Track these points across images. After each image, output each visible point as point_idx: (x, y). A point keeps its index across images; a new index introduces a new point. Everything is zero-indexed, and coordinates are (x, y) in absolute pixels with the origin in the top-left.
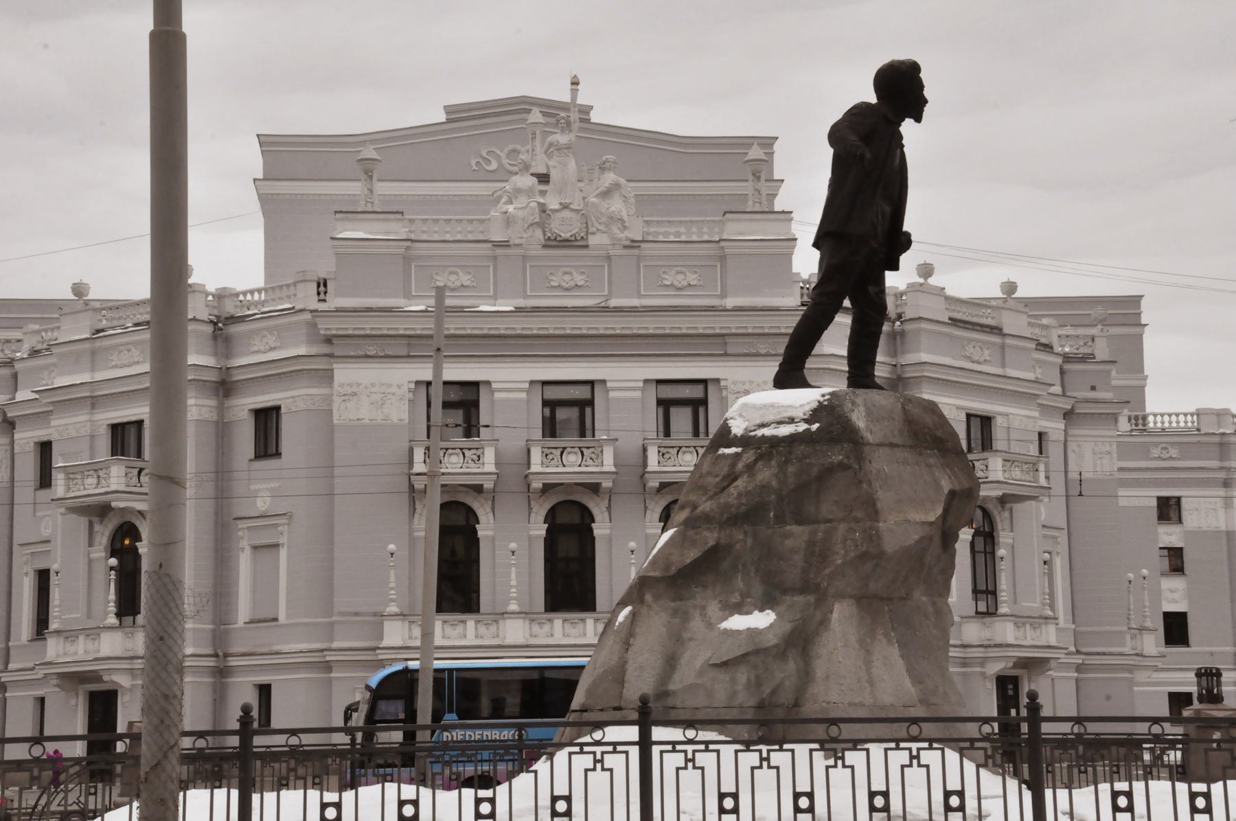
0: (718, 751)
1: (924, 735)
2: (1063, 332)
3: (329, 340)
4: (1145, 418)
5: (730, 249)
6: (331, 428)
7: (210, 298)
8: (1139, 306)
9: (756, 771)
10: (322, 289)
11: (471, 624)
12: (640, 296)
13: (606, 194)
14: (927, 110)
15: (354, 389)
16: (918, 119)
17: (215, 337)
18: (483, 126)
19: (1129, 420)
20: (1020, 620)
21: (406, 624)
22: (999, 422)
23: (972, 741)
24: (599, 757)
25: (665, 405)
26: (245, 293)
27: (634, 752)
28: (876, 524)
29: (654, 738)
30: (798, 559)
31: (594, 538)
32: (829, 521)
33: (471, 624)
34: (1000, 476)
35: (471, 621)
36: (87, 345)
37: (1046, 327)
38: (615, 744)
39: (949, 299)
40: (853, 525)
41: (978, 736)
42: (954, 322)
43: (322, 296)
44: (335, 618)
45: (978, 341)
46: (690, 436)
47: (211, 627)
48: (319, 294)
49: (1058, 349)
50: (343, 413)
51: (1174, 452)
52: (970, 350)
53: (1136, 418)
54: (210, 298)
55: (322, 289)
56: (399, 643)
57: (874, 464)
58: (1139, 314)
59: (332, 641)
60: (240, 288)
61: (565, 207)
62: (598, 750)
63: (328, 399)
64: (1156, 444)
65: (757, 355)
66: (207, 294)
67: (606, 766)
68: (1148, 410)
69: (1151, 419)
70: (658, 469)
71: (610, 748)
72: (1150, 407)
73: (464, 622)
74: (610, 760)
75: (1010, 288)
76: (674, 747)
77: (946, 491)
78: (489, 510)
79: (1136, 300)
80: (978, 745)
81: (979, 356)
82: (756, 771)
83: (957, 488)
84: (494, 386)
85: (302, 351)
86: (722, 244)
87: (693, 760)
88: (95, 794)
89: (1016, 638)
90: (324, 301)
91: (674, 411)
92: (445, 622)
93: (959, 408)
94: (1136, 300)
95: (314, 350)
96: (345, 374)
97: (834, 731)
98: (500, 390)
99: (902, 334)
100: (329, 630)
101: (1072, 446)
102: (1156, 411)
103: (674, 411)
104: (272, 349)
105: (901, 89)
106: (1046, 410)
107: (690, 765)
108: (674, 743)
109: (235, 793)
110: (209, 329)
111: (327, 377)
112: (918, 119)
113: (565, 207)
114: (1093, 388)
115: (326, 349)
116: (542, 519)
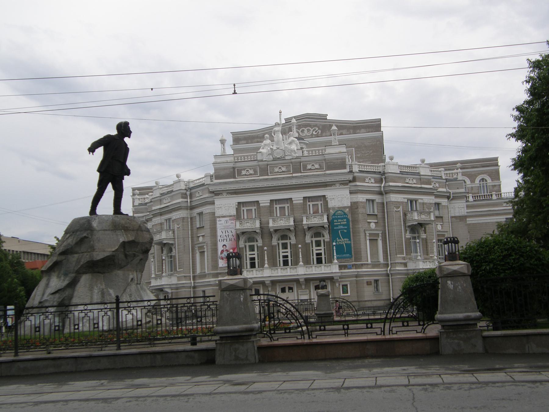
4: (501, 194)
8: (497, 160)
12: (301, 173)
13: (290, 143)
14: (132, 135)
15: (333, 197)
16: (129, 137)
27: (115, 311)
29: (120, 306)
30: (74, 263)
33: (254, 271)
34: (416, 218)
36: (159, 198)
37: (440, 171)
38: (90, 310)
49: (444, 178)
51: (505, 205)
56: (304, 273)
60: (194, 179)
61: (278, 148)
68: (502, 191)
69: (503, 194)
75: (423, 161)
83: (126, 240)
85: (207, 195)
93: (404, 198)
94: (496, 159)
97: (129, 304)
105: (124, 129)
106: (437, 196)
108: (102, 309)
111: (213, 203)
112: (129, 137)
113: (278, 148)
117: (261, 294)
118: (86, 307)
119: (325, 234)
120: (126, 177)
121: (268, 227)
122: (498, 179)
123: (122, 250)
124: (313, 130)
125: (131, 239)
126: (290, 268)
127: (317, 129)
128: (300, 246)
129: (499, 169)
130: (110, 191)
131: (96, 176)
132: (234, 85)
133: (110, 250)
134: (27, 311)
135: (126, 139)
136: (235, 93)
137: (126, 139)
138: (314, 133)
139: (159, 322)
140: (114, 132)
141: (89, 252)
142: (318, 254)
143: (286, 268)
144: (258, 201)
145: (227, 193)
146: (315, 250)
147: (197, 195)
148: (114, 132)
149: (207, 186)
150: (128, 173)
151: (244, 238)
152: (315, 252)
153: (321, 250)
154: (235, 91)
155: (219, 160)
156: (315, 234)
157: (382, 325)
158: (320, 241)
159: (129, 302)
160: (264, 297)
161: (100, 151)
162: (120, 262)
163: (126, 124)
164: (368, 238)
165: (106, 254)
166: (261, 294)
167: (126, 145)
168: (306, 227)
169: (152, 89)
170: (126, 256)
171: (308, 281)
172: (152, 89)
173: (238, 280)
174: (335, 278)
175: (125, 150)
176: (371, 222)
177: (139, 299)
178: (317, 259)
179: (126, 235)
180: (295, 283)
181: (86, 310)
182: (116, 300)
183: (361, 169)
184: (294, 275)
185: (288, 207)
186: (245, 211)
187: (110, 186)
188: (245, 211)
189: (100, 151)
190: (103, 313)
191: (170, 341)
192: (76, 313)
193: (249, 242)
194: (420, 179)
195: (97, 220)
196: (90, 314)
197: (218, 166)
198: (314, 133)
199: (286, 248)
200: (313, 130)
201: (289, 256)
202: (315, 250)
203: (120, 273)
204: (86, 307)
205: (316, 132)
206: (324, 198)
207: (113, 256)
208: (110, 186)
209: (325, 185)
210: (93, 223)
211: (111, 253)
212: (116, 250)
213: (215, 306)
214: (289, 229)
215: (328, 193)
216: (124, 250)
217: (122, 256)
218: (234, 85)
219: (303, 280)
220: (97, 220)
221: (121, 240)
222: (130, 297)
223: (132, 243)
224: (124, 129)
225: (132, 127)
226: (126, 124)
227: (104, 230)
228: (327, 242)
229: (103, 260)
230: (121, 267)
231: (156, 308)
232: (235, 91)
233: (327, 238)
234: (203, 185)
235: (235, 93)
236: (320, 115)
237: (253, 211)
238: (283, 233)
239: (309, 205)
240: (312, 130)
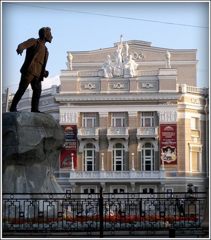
0: (19, 201)
1: (14, 198)
5: (160, 78)
9: (48, 206)
10: (58, 89)
18: (142, 48)
23: (8, 199)
24: (12, 202)
28: (18, 146)
32: (7, 146)
38: (17, 199)
40: (13, 146)
41: (49, 198)
43: (58, 91)
48: (57, 91)
55: (58, 89)
57: (20, 131)
62: (12, 200)
67: (194, 204)
70: (119, 135)
71: (15, 200)
74: (54, 203)
76: (168, 200)
77: (42, 138)
78: (98, 145)
80: (189, 199)
82: (48, 206)
83: (47, 137)
84: (128, 113)
85: (53, 104)
86: (158, 77)
87: (13, 204)
88: (167, 210)
90: (58, 92)
98: (101, 115)
105: (45, 35)
107: (192, 204)
108: (27, 199)
117: (155, 193)
119: (154, 145)
121: (106, 135)
123: (42, 146)
125: (50, 136)
126: (94, 173)
128: (133, 154)
133: (33, 144)
135: (47, 44)
139: (22, 215)
141: (14, 145)
142: (147, 162)
143: (120, 173)
144: (98, 113)
145: (71, 104)
146: (145, 158)
148: (37, 37)
149: (53, 97)
151: (84, 144)
152: (145, 160)
153: (150, 158)
155: (65, 74)
156: (87, 145)
158: (150, 150)
159: (51, 194)
160: (128, 196)
161: (25, 51)
162: (40, 157)
163: (48, 29)
164: (191, 150)
165: (29, 148)
166: (155, 193)
167: (46, 49)
168: (139, 138)
170: (45, 151)
171: (138, 184)
174: (162, 183)
176: (194, 137)
177: (53, 192)
178: (88, 166)
179: (46, 132)
180: (126, 186)
181: (12, 199)
183: (188, 91)
184: (80, 179)
185: (124, 119)
186: (86, 120)
188: (86, 120)
190: (28, 203)
191: (70, 233)
192: (181, 202)
193: (87, 148)
195: (21, 117)
196: (17, 204)
197: (64, 79)
199: (91, 155)
201: (122, 162)
202: (145, 158)
203: (38, 166)
204: (12, 197)
206: (155, 114)
207: (35, 150)
209: (158, 102)
210: (17, 119)
211: (34, 147)
212: (38, 145)
213: (158, 202)
214: (94, 139)
215: (160, 109)
216: (44, 146)
217: (41, 151)
219: (134, 184)
220: (21, 117)
221: (42, 136)
222: (47, 189)
223: (51, 139)
224: (45, 35)
226: (48, 29)
227: (27, 126)
228: (156, 152)
229: (26, 154)
230: (39, 161)
231: (160, 201)
233: (156, 148)
234: (50, 95)
236: (145, 42)
237: (93, 120)
238: (148, 142)
239: (142, 119)
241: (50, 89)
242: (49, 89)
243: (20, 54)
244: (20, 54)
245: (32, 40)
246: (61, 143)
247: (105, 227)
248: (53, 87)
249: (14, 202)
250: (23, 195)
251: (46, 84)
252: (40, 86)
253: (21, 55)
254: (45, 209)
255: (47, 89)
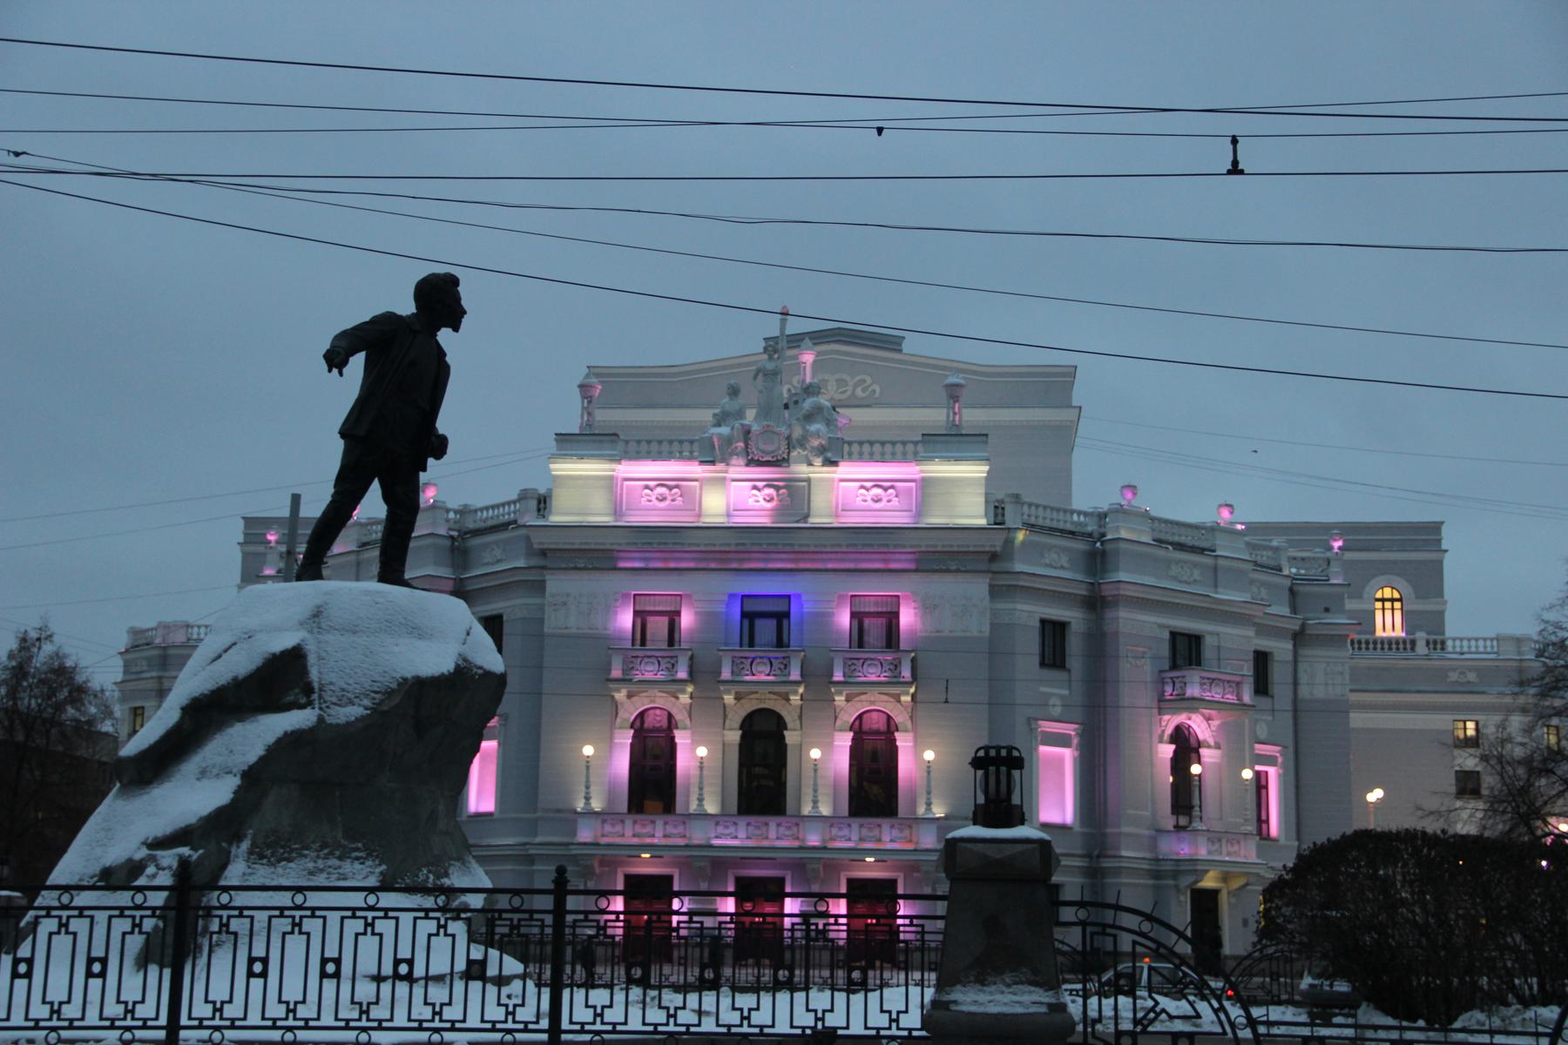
2: (1293, 553)
3: (543, 553)
4: (1443, 643)
6: (541, 636)
7: (452, 515)
11: (659, 824)
14: (465, 320)
16: (456, 329)
17: (453, 549)
19: (1428, 643)
20: (1215, 837)
21: (599, 821)
22: (1209, 641)
25: (749, 617)
26: (481, 510)
29: (569, 906)
31: (785, 746)
35: (773, 822)
36: (353, 558)
39: (1153, 519)
42: (1160, 542)
44: (539, 814)
45: (496, 543)
46: (665, 646)
47: (1109, 830)
50: (554, 622)
52: (1175, 570)
53: (1435, 642)
54: (452, 515)
58: (1439, 541)
59: (536, 835)
60: (479, 505)
63: (541, 608)
64: (1454, 670)
65: (948, 571)
66: (448, 511)
68: (1448, 634)
69: (1449, 643)
72: (1451, 630)
73: (653, 822)
79: (1436, 527)
81: (1184, 578)
85: (521, 563)
89: (1209, 853)
91: (759, 623)
92: (861, 826)
93: (1161, 626)
94: (1436, 527)
95: (534, 562)
96: (556, 584)
99: (1103, 553)
100: (533, 827)
101: (1302, 667)
102: (1470, 635)
103: (759, 623)
104: (499, 561)
105: (440, 300)
106: (1263, 630)
109: (167, 973)
110: (448, 543)
111: (540, 587)
112: (456, 329)
114: (1327, 610)
115: (541, 562)
116: (737, 725)
118: (299, 899)
120: (431, 461)
122: (1439, 592)
124: (856, 386)
127: (869, 380)
129: (1440, 562)
130: (372, 506)
131: (331, 454)
132: (1234, 141)
134: (225, 898)
135: (445, 336)
136: (1235, 170)
137: (445, 336)
138: (859, 392)
140: (406, 306)
143: (653, 822)
147: (487, 558)
148: (406, 306)
149: (523, 531)
150: (439, 447)
154: (1235, 163)
157: (163, 1021)
161: (358, 362)
167: (441, 354)
169: (880, 130)
172: (880, 130)
173: (1019, 847)
175: (438, 373)
182: (556, 882)
187: (375, 488)
189: (358, 362)
194: (1215, 569)
198: (859, 392)
200: (856, 386)
205: (864, 390)
208: (375, 488)
218: (1234, 141)
224: (440, 300)
225: (467, 295)
232: (1235, 163)
235: (1235, 170)
240: (851, 383)
241: (514, 502)
242: (509, 503)
243: (335, 371)
244: (335, 371)
245: (387, 322)
246: (1426, 651)
247: (1191, 998)
248: (524, 496)
249: (194, 1015)
250: (88, 1006)
251: (440, 485)
252: (414, 490)
253: (341, 374)
254: (619, 997)
255: (503, 505)
